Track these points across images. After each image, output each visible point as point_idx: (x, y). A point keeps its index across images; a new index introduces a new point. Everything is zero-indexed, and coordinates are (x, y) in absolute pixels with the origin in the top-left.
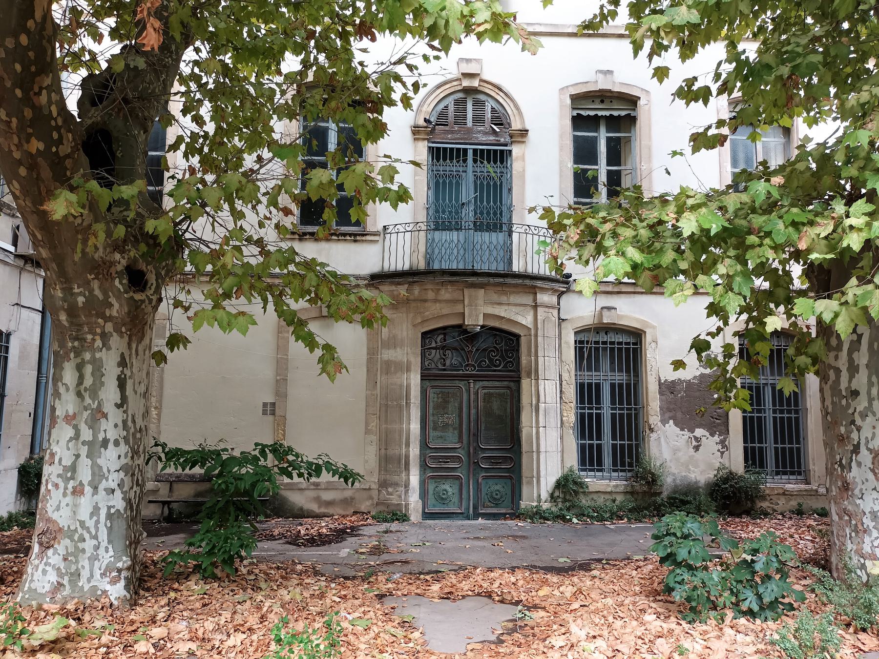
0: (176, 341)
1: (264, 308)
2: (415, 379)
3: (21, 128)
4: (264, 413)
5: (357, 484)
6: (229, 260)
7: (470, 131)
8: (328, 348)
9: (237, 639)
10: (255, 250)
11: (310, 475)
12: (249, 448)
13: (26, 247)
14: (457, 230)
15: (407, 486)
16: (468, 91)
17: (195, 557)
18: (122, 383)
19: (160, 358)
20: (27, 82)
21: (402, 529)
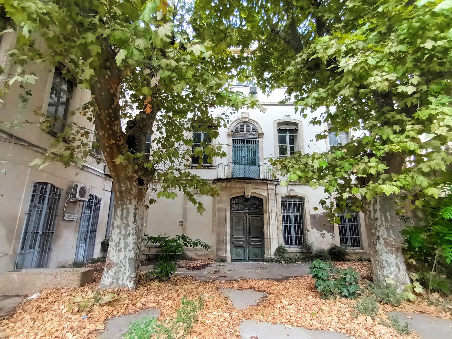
0: (152, 201)
1: (180, 191)
3: (109, 135)
4: (179, 225)
6: (170, 176)
8: (200, 204)
9: (169, 302)
10: (178, 172)
15: (226, 250)
16: (244, 122)
18: (135, 215)
19: (147, 207)
20: (111, 123)
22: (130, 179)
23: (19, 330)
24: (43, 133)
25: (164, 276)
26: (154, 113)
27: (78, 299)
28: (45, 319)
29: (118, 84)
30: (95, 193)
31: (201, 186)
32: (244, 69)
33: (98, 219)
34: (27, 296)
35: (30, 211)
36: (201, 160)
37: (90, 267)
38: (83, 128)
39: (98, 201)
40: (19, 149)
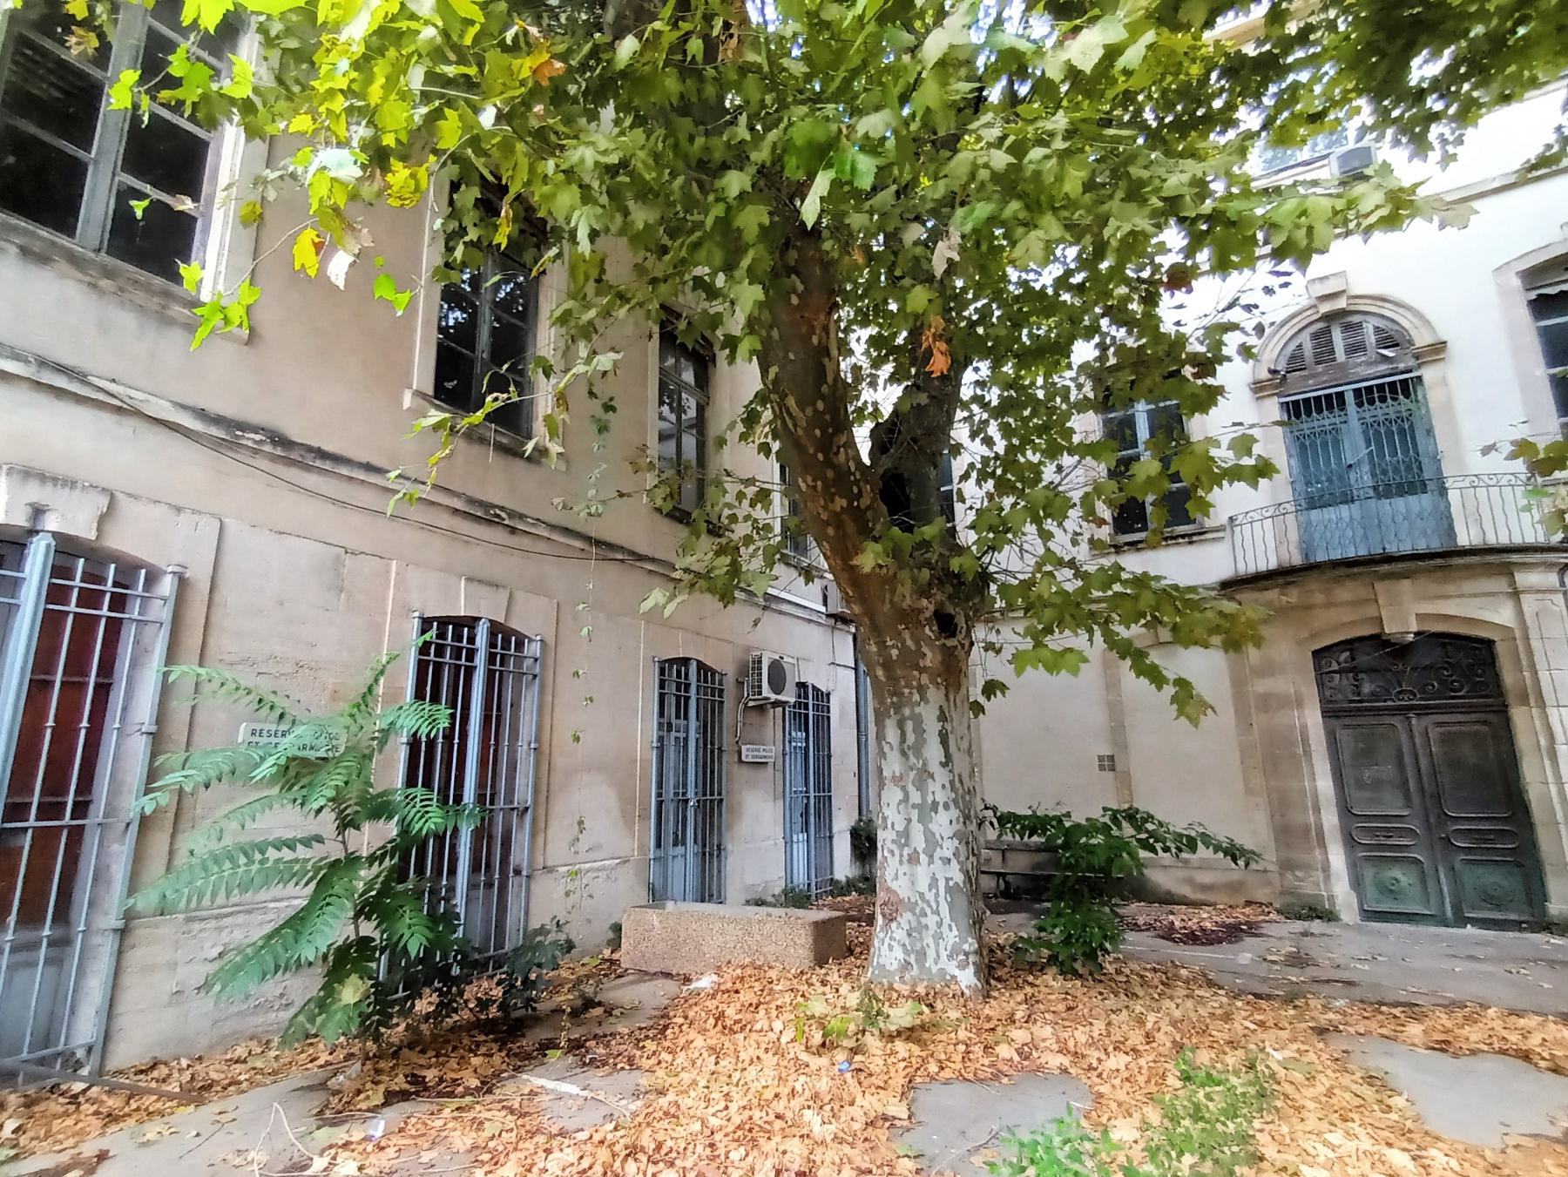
0: (991, 688)
1: (1091, 640)
2: (1313, 718)
3: (826, 487)
4: (1102, 768)
5: (1253, 866)
6: (1045, 589)
7: (1343, 366)
8: (1182, 683)
9: (1118, 1061)
10: (1068, 573)
11: (1180, 850)
12: (1097, 814)
13: (837, 606)
14: (1346, 502)
15: (1326, 868)
16: (1330, 317)
17: (1049, 945)
18: (944, 742)
19: (978, 709)
20: (826, 445)
21: (1329, 931)
22: (909, 617)
23: (686, 1077)
24: (657, 515)
25: (1081, 957)
26: (952, 379)
27: (818, 1007)
28: (743, 1056)
29: (829, 314)
30: (810, 680)
31: (1174, 612)
32: (1296, 86)
33: (829, 757)
34: (687, 980)
35: (661, 739)
36: (1176, 510)
37: (832, 907)
38: (750, 481)
39: (823, 697)
40: (612, 572)
